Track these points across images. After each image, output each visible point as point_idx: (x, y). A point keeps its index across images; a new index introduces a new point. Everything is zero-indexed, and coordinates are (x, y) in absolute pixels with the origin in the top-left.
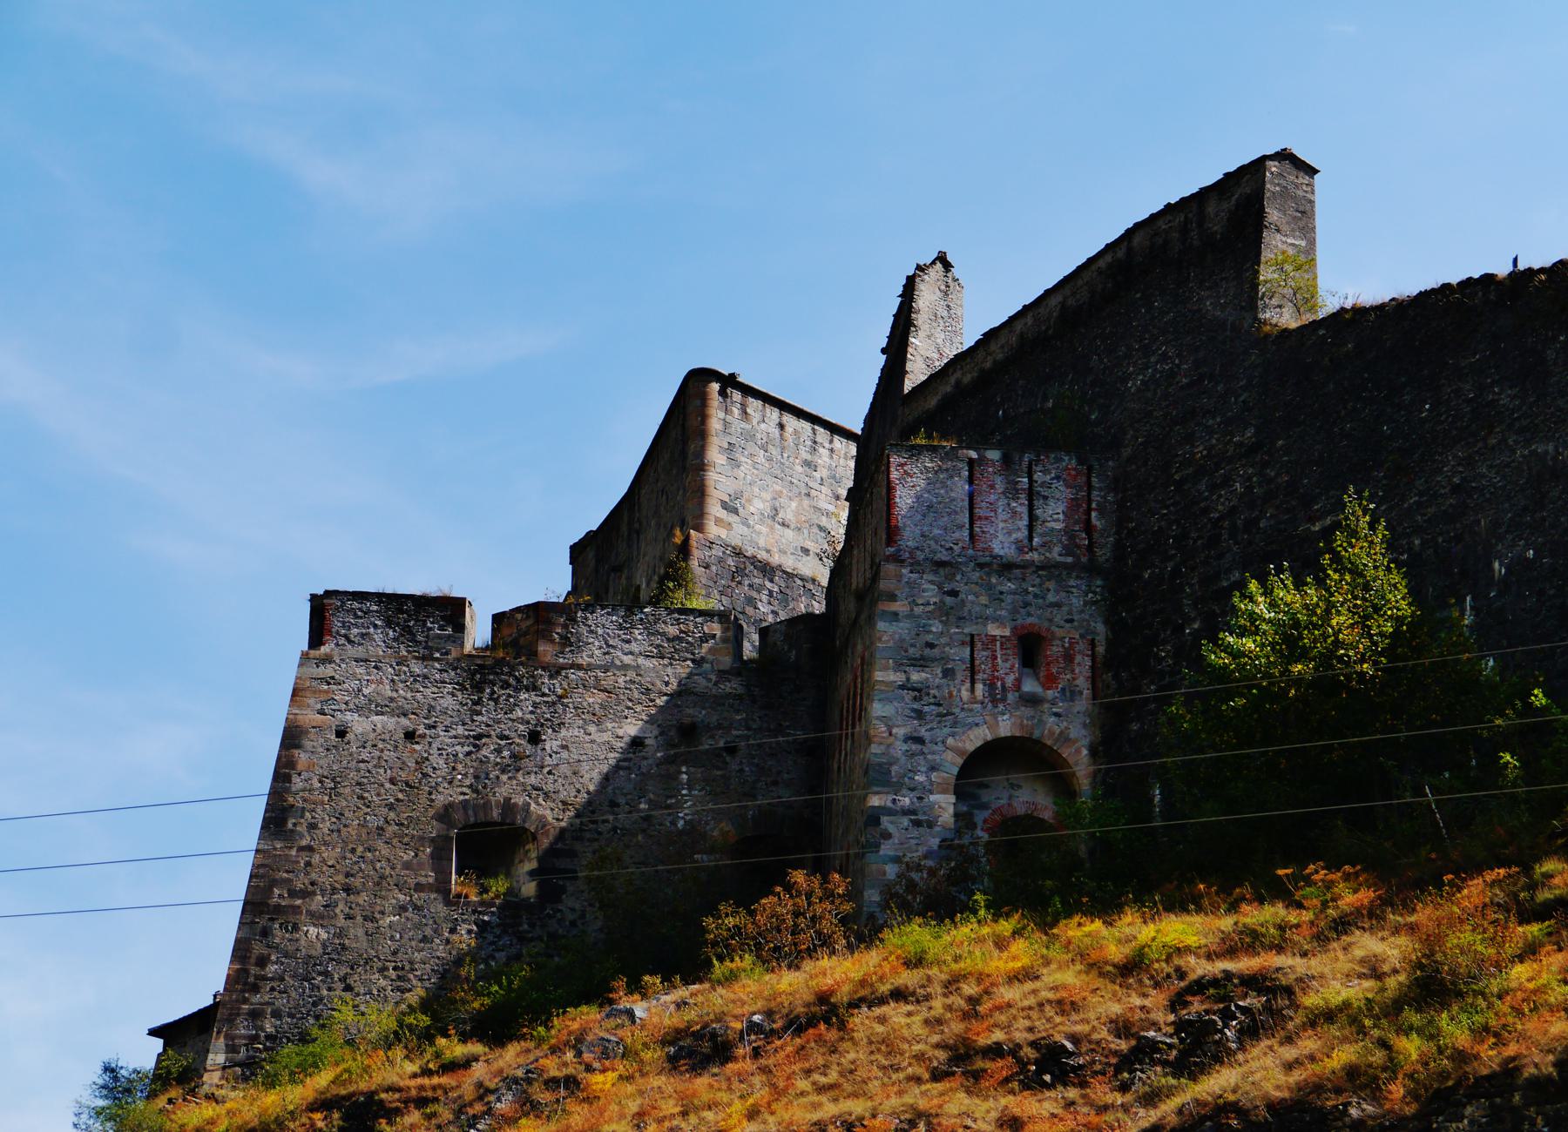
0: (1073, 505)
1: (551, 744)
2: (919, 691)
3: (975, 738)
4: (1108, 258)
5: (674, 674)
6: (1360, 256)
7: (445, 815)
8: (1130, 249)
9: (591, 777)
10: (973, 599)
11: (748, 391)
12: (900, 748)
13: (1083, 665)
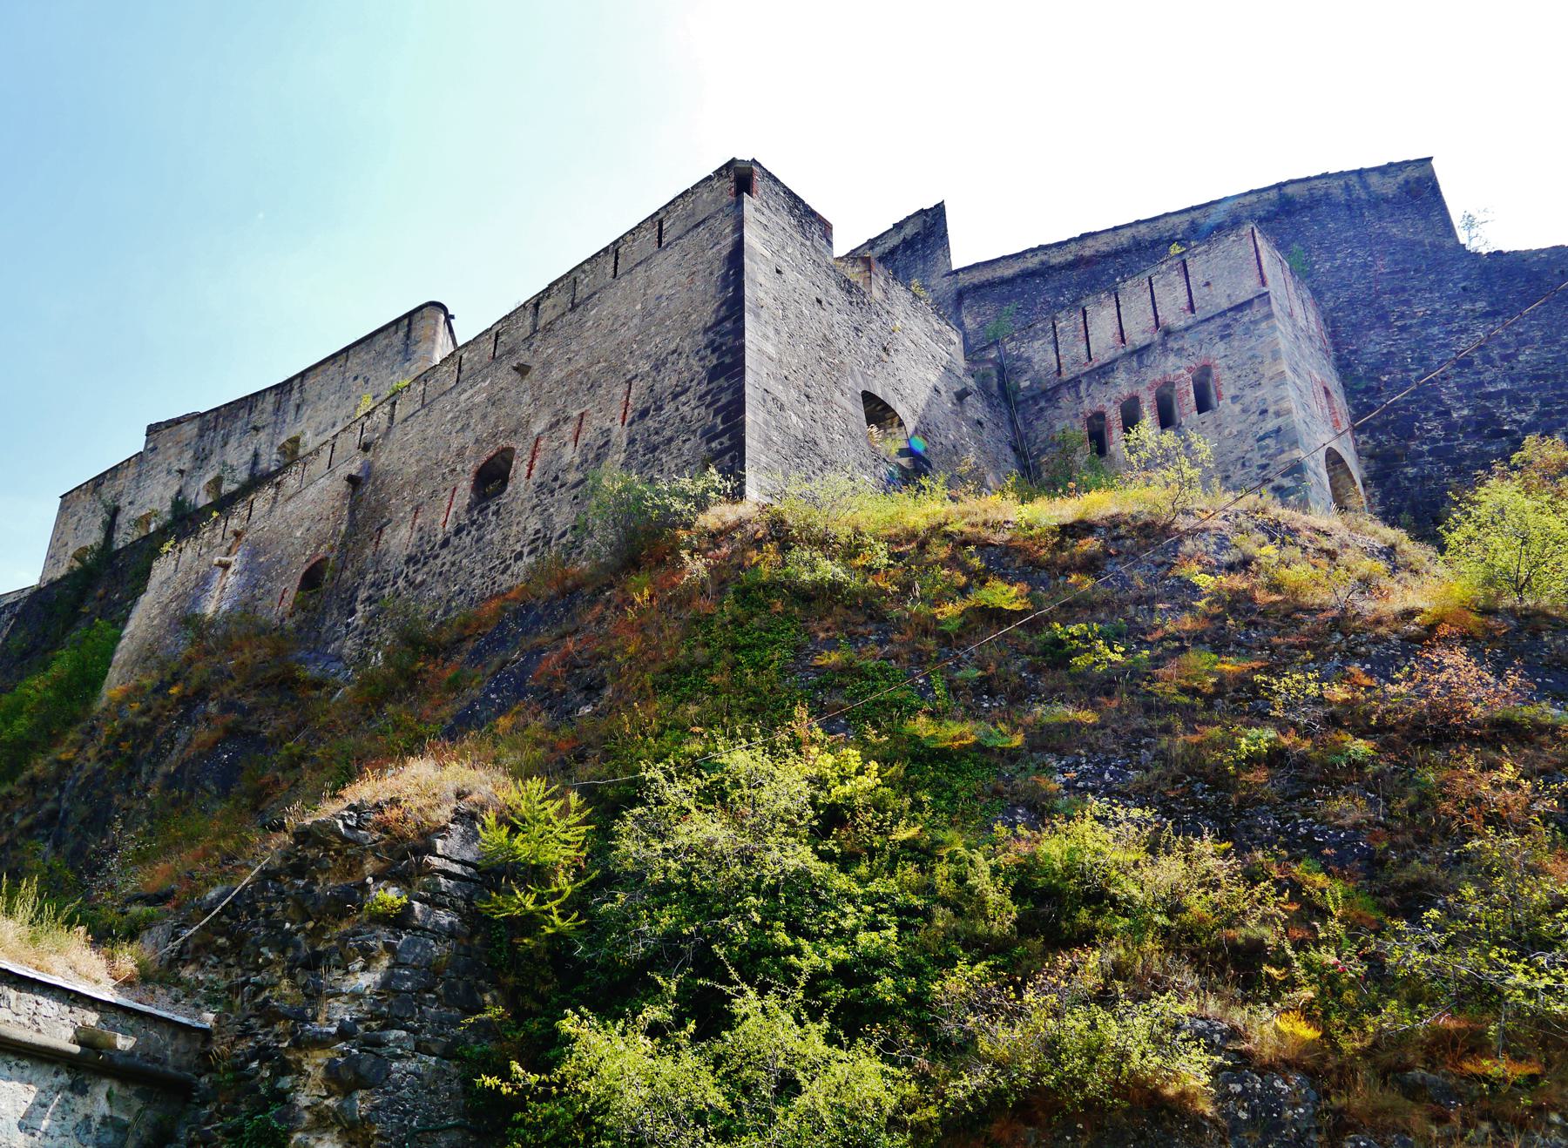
4: (1254, 198)
8: (1282, 196)
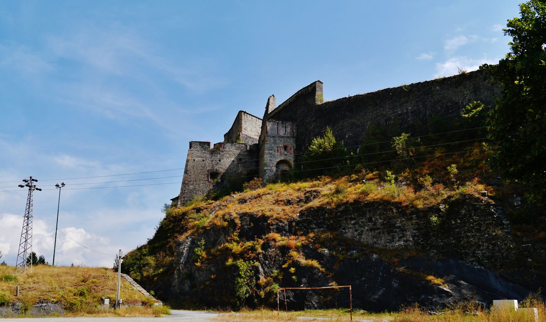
0: (291, 128)
1: (222, 161)
2: (271, 154)
3: (278, 160)
5: (238, 152)
6: (328, 95)
7: (208, 171)
9: (227, 166)
10: (278, 141)
11: (247, 114)
12: (268, 161)
13: (292, 150)
